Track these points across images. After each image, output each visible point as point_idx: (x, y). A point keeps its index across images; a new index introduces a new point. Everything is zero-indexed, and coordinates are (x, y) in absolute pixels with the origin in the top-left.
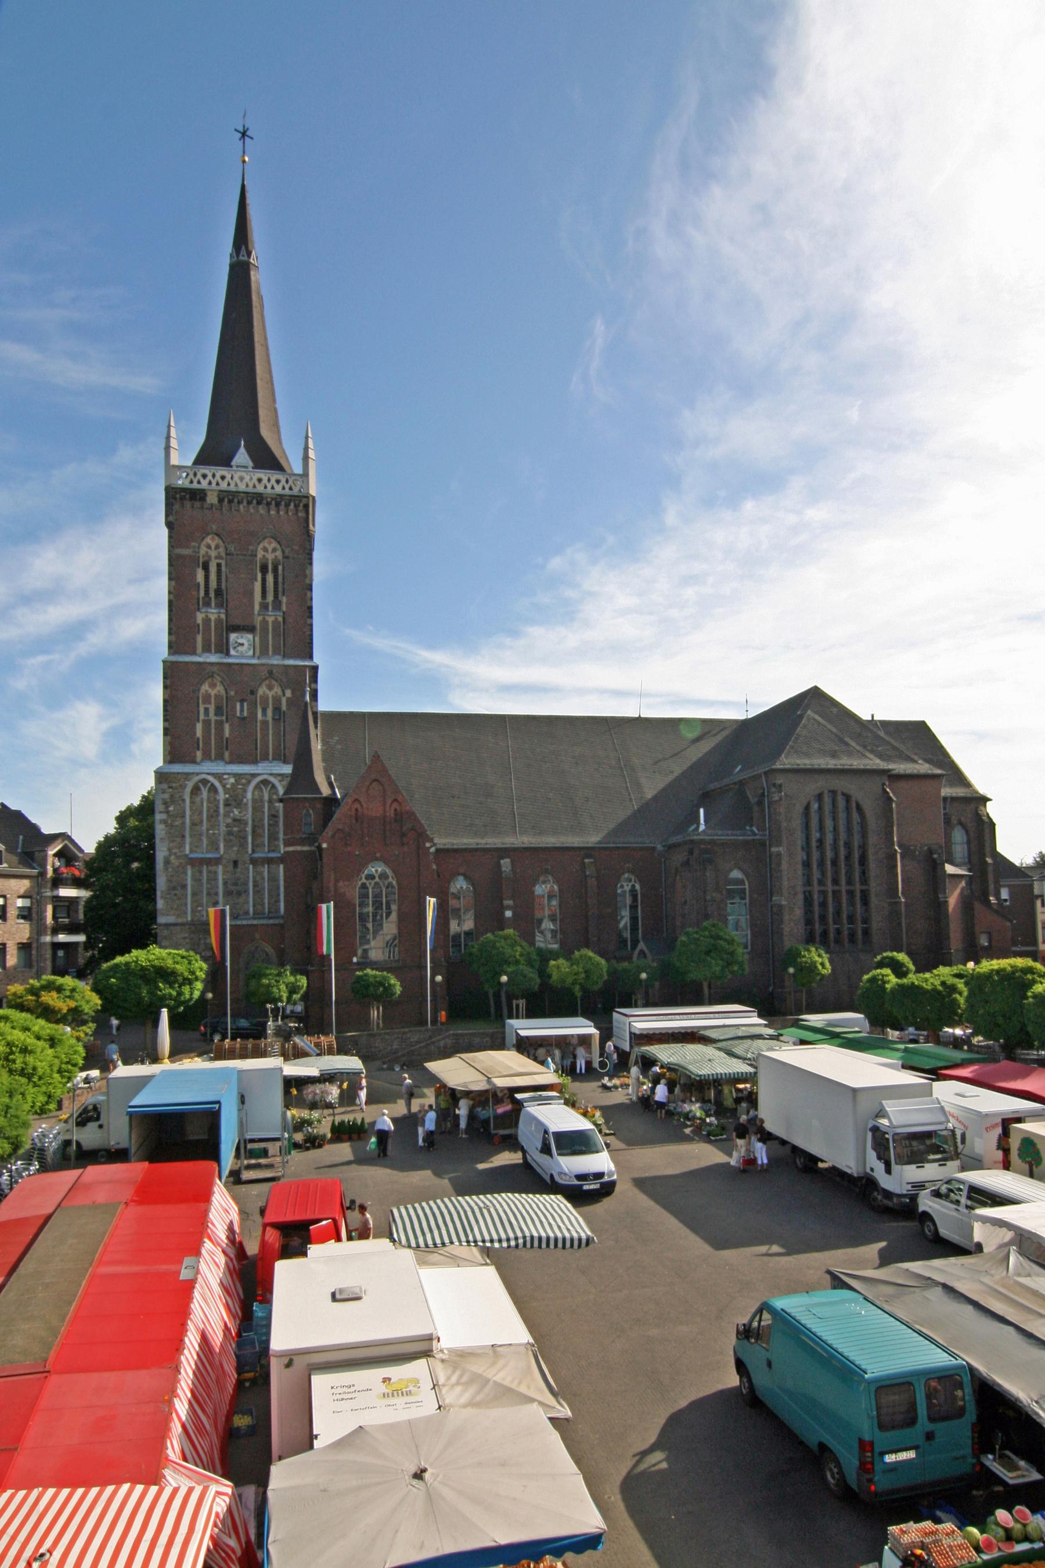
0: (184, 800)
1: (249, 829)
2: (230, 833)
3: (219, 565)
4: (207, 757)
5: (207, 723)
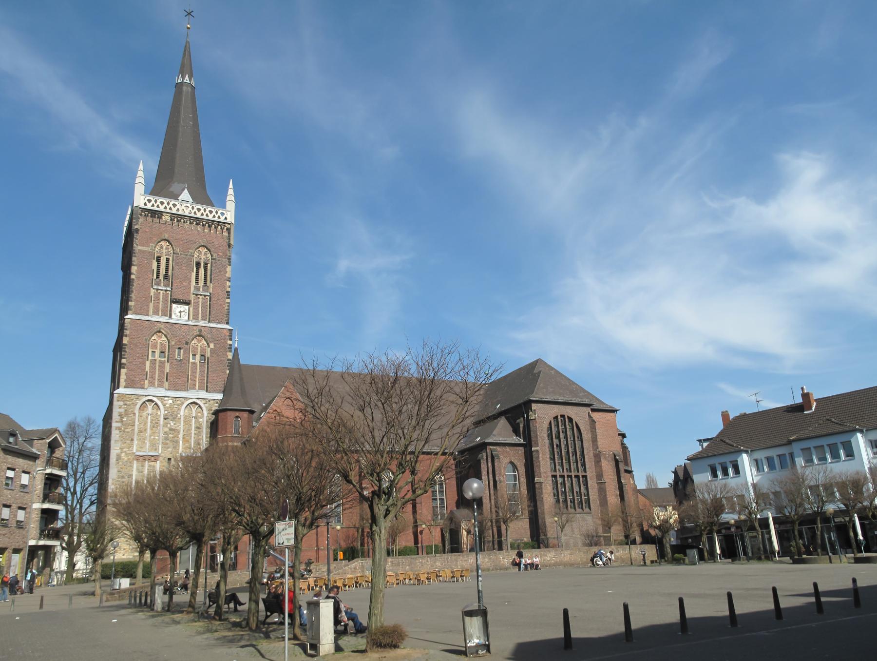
0: (134, 414)
1: (181, 436)
2: (166, 439)
3: (168, 260)
4: (152, 384)
5: (153, 362)
